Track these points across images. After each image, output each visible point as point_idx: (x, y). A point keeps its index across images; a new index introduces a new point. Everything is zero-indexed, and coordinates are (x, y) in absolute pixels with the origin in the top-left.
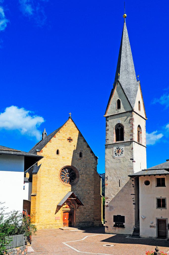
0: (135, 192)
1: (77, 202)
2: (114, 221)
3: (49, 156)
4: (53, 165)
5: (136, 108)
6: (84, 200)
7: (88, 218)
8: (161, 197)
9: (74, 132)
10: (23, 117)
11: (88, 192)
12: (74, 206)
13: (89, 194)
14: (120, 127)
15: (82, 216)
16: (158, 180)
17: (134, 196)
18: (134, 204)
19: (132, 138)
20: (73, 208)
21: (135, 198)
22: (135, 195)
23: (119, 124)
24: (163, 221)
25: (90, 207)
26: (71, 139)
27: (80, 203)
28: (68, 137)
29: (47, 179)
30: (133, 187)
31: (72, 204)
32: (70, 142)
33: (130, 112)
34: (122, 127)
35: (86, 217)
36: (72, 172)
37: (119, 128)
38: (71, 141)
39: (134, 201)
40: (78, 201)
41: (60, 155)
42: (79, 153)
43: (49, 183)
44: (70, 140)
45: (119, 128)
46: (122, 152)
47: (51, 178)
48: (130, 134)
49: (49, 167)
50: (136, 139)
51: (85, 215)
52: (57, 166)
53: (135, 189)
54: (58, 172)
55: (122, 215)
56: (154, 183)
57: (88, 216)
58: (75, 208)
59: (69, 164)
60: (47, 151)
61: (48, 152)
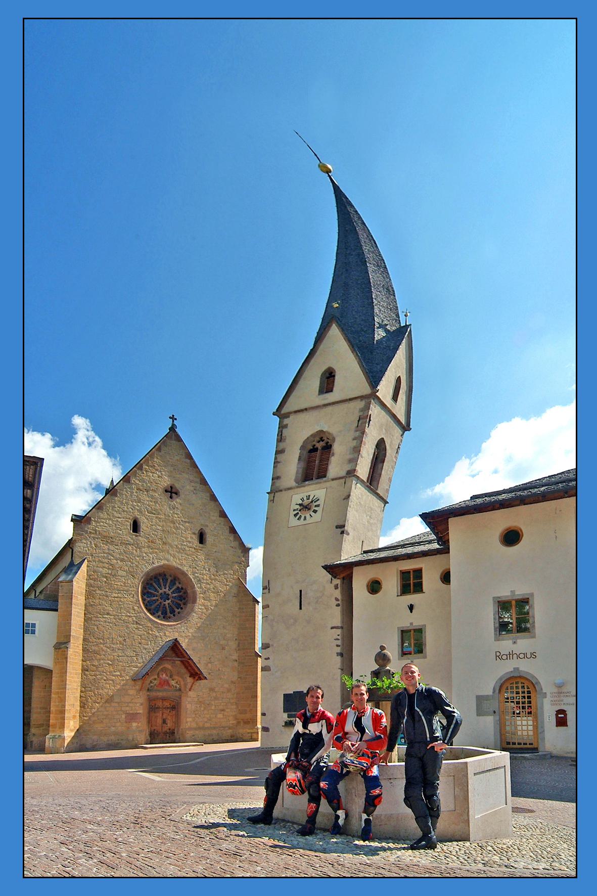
0: (343, 622)
1: (189, 671)
7: (220, 716)
8: (411, 624)
13: (223, 649)
16: (404, 575)
17: (339, 631)
21: (343, 638)
22: (342, 628)
30: (338, 605)
32: (171, 497)
37: (319, 445)
39: (338, 646)
43: (108, 614)
44: (171, 492)
45: (319, 445)
48: (351, 456)
50: (363, 470)
51: (213, 708)
57: (223, 710)
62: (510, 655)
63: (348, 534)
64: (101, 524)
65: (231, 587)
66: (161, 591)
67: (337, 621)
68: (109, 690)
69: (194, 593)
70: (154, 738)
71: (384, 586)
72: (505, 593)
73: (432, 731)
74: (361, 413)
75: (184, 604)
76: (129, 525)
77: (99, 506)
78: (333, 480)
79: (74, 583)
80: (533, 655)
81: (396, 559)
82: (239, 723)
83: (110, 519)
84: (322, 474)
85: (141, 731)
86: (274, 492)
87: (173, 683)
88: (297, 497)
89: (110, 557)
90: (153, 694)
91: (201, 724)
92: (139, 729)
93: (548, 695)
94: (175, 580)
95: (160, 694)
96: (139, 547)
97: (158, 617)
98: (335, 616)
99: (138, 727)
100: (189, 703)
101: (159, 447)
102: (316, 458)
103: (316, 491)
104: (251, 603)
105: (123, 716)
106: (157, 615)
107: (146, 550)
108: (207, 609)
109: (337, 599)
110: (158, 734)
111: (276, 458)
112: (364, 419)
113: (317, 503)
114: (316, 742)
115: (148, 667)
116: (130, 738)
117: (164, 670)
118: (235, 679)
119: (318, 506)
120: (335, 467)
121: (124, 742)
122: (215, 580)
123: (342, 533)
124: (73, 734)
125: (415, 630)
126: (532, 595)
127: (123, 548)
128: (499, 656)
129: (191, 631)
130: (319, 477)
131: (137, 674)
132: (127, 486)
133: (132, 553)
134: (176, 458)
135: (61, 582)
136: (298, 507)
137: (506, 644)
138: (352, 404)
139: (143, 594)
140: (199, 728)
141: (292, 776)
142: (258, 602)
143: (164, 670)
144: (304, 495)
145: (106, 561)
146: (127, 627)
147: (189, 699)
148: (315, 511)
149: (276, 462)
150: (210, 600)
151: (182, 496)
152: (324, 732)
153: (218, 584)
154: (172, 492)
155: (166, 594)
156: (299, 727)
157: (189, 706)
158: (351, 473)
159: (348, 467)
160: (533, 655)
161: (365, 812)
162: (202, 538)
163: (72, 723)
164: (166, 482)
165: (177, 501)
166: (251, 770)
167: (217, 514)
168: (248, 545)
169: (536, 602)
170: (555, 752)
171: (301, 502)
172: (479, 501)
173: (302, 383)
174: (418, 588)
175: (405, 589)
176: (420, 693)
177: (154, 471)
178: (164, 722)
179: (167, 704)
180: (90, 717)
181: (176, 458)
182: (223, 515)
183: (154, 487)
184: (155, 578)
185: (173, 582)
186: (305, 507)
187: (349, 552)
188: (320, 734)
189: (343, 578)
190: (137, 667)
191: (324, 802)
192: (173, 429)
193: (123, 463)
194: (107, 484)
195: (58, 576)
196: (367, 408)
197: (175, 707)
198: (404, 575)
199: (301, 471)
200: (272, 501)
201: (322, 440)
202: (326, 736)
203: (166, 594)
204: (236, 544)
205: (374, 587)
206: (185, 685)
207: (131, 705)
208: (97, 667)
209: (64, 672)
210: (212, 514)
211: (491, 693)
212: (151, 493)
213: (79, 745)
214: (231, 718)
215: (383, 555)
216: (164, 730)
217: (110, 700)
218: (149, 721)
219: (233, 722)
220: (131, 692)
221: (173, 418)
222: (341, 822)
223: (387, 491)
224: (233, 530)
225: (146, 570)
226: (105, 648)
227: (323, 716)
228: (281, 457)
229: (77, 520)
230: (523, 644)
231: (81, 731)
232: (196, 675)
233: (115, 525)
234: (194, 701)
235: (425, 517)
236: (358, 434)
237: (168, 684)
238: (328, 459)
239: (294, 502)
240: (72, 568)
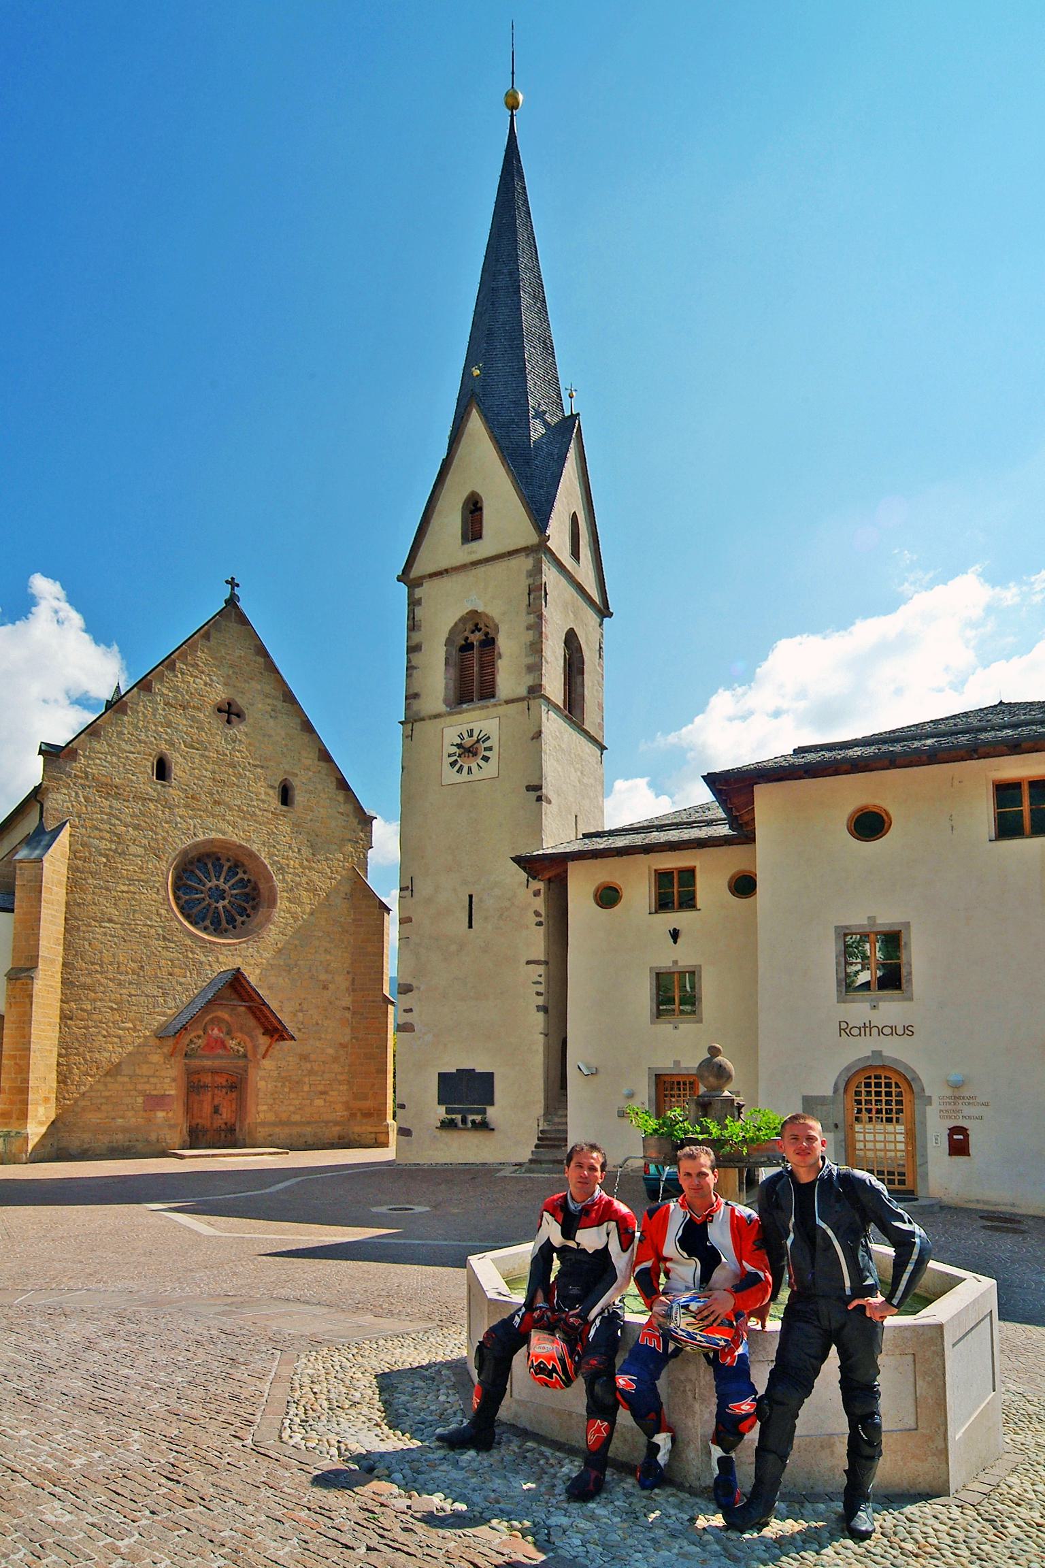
0: (547, 953)
1: (262, 1024)
2: (441, 1101)
8: (675, 962)
10: (67, 693)
11: (323, 977)
12: (249, 1045)
14: (480, 630)
15: (292, 1096)
16: (663, 878)
17: (541, 969)
18: (539, 1008)
19: (537, 682)
20: (245, 1056)
22: (546, 963)
23: (474, 613)
24: (685, 1084)
25: (331, 1051)
27: (276, 1024)
30: (539, 924)
31: (239, 1035)
32: (229, 722)
33: (527, 555)
34: (487, 634)
35: (312, 1100)
36: (241, 875)
37: (476, 638)
39: (538, 994)
40: (266, 1016)
42: (277, 784)
43: (110, 921)
44: (229, 713)
45: (476, 638)
46: (487, 754)
48: (530, 660)
49: (111, 841)
51: (306, 1088)
53: (548, 935)
55: (479, 1069)
56: (639, 891)
57: (322, 1093)
58: (255, 1055)
62: (866, 1029)
63: (549, 802)
64: (97, 762)
65: (339, 883)
66: (209, 885)
67: (539, 952)
68: (111, 1053)
69: (272, 889)
70: (197, 1138)
71: (626, 894)
72: (857, 919)
73: (858, 1273)
74: (531, 581)
75: (254, 908)
76: (149, 765)
77: (91, 730)
78: (507, 702)
79: (45, 864)
80: (908, 1030)
81: (647, 849)
82: (353, 1115)
83: (113, 754)
84: (487, 692)
85: (171, 1127)
86: (411, 720)
87: (232, 1043)
88: (452, 731)
89: (114, 821)
90: (196, 1063)
91: (284, 1116)
92: (169, 1121)
93: (935, 1100)
94: (236, 866)
95: (208, 1063)
96: (168, 806)
97: (205, 929)
98: (536, 943)
99: (166, 1119)
100: (263, 1078)
101: (205, 633)
102: (474, 663)
103: (481, 721)
104: (377, 911)
105: (140, 1100)
106: (202, 925)
107: (182, 811)
108: (296, 919)
109: (537, 914)
110: (205, 1131)
111: (409, 661)
112: (536, 592)
113: (487, 744)
114: (597, 1271)
115: (187, 1016)
116: (153, 1137)
117: (217, 1021)
118: (346, 1039)
119: (490, 749)
120: (508, 680)
121: (140, 1146)
122: (310, 868)
123: (539, 799)
124: (43, 1129)
125: (680, 973)
126: (907, 925)
128: (845, 1029)
129: (266, 955)
130: (483, 697)
131: (164, 1027)
132: (144, 697)
133: (156, 816)
134: (238, 653)
135: (20, 861)
136: (455, 749)
137: (858, 1010)
139: (176, 888)
140: (281, 1123)
141: (544, 1346)
142: (388, 910)
143: (217, 1021)
144: (463, 730)
145: (107, 827)
146: (147, 945)
147: (261, 1073)
148: (486, 759)
149: (410, 668)
150: (300, 904)
151: (250, 719)
152: (614, 1248)
153: (315, 877)
154: (230, 712)
155: (220, 888)
156: (552, 1230)
157: (262, 1084)
158: (535, 691)
159: (529, 680)
160: (908, 1030)
161: (718, 1439)
162: (286, 795)
163: (41, 1110)
164: (219, 693)
165: (239, 730)
166: (383, 1209)
167: (314, 755)
168: (370, 812)
169: (913, 940)
170: (947, 1200)
171: (459, 741)
172: (811, 757)
174: (688, 903)
175: (663, 904)
176: (827, 1182)
177: (196, 673)
178: (216, 1110)
179: (221, 1080)
180: (76, 1101)
181: (238, 653)
182: (325, 756)
183: (196, 701)
184: (199, 860)
185: (233, 871)
186: (468, 751)
187: (556, 837)
188: (604, 1253)
189: (549, 880)
190: (164, 1014)
191: (624, 1417)
192: (232, 602)
193: (128, 657)
194: (107, 694)
195: (14, 850)
196: (537, 571)
197: (237, 1085)
198: (663, 878)
199: (451, 684)
200: (408, 737)
201: (477, 628)
202: (620, 1260)
203: (220, 888)
204: (349, 808)
205: (608, 897)
206: (255, 1047)
207: (152, 1080)
208: (89, 1013)
209: (25, 1021)
211: (830, 1093)
212: (191, 711)
213: (56, 1148)
214: (339, 1107)
215: (621, 842)
216: (215, 1126)
217: (114, 1071)
218: (188, 1110)
219: (340, 1113)
220: (155, 1058)
221: (232, 583)
222: (662, 1458)
223: (601, 726)
224: (343, 785)
225: (181, 846)
226: (104, 981)
227: (607, 1213)
228: (417, 659)
229: (50, 753)
230: (890, 1009)
231: (59, 1124)
232: (276, 1031)
233: (125, 760)
234: (268, 1073)
235: (711, 780)
237: (223, 1045)
238: (492, 664)
239: (447, 742)
240: (42, 837)
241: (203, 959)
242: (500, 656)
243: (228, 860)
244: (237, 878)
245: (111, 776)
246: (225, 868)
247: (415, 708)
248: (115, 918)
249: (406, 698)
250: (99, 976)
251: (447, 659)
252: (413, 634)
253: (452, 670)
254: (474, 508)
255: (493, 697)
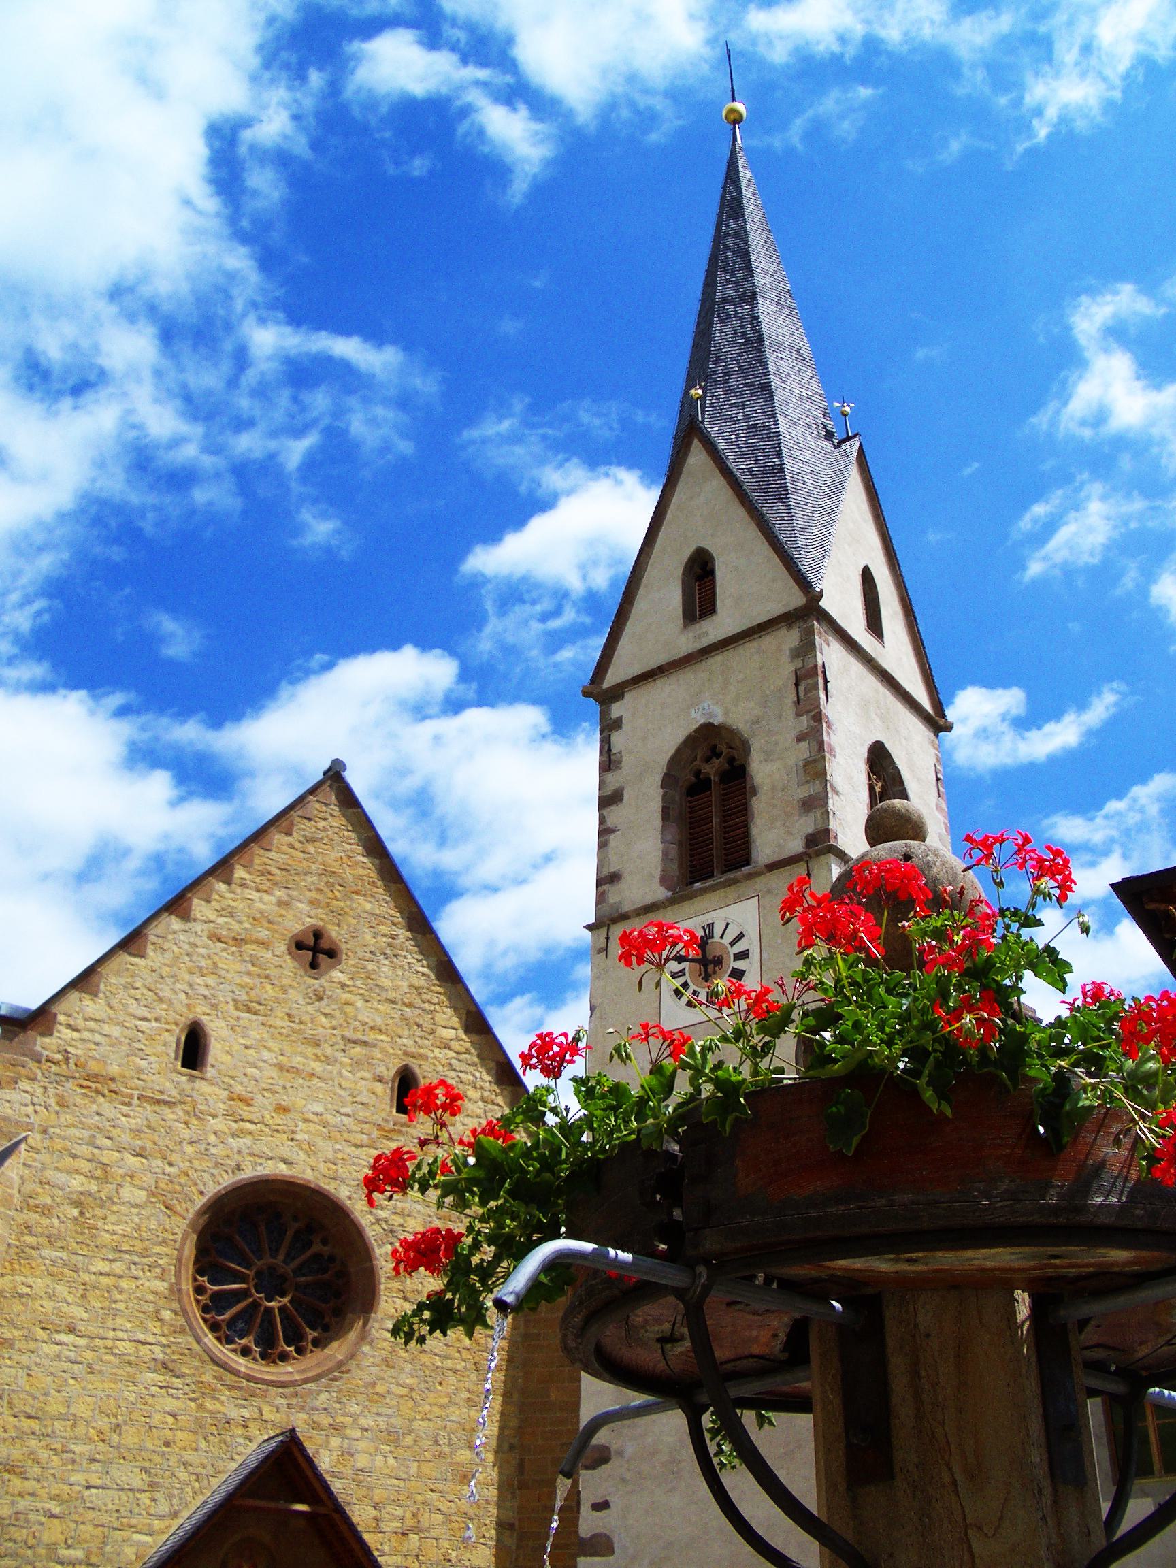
3: (114, 1069)
4: (133, 1161)
5: (841, 600)
6: (414, 1537)
9: (357, 893)
14: (718, 756)
19: (820, 826)
26: (324, 944)
28: (301, 918)
29: (62, 1290)
34: (731, 760)
36: (315, 1248)
37: (711, 770)
38: (322, 958)
41: (210, 1072)
43: (71, 1330)
45: (711, 770)
46: (740, 965)
47: (104, 1280)
48: (805, 792)
52: (168, 1169)
54: (174, 1234)
59: (285, 1162)
60: (92, 1024)
61: (98, 1038)
74: (798, 663)
76: (171, 1041)
78: (772, 867)
97: (245, 1352)
111: (602, 820)
112: (808, 680)
127: (140, 1115)
138: (768, 642)
145: (84, 1150)
154: (315, 950)
159: (806, 825)
173: (641, 605)
196: (807, 647)
199: (674, 851)
201: (714, 753)
210: (440, 1018)
225: (212, 1190)
226: (44, 1455)
236: (805, 722)
241: (234, 1413)
242: (754, 792)
243: (296, 1218)
244: (308, 1254)
245: (103, 1061)
246: (289, 1234)
247: (613, 899)
248: (81, 1327)
249: (599, 883)
250: (33, 1443)
251: (665, 810)
252: (610, 777)
253: (673, 828)
254: (700, 573)
255: (748, 864)
